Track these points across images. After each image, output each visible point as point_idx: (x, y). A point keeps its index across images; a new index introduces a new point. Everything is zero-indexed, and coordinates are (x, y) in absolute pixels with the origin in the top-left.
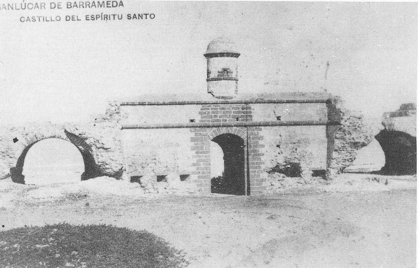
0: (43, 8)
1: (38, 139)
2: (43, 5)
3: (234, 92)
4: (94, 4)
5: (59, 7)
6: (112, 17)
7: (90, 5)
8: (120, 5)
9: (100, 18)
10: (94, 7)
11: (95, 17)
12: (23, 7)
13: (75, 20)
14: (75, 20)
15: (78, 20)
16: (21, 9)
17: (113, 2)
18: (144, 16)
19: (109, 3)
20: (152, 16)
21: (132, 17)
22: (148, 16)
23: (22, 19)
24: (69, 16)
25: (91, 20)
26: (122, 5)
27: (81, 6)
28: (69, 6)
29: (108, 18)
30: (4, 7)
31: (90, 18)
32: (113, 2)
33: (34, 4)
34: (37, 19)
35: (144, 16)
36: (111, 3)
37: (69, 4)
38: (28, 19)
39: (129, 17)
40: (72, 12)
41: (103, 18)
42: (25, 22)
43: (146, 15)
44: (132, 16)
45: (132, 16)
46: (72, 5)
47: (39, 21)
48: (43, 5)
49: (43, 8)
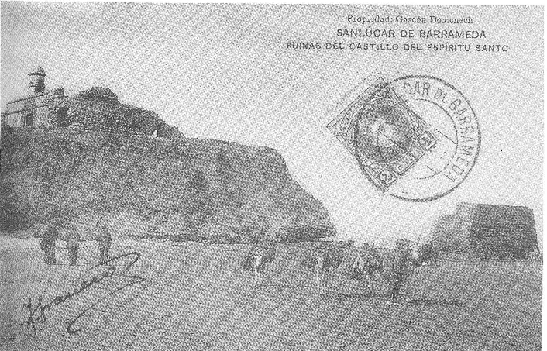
0: (392, 36)
3: (467, 111)
4: (346, 32)
5: (411, 35)
6: (458, 47)
7: (447, 35)
8: (481, 36)
10: (430, 36)
11: (439, 47)
12: (369, 34)
17: (473, 32)
18: (496, 48)
24: (330, 44)
25: (433, 50)
26: (484, 36)
27: (437, 36)
28: (423, 35)
29: (454, 48)
30: (430, 34)
31: (433, 48)
32: (473, 32)
33: (382, 31)
35: (496, 48)
36: (471, 33)
37: (422, 32)
38: (485, 48)
41: (448, 48)
42: (356, 49)
43: (498, 46)
44: (482, 48)
45: (482, 48)
47: (461, 50)
49: (392, 36)
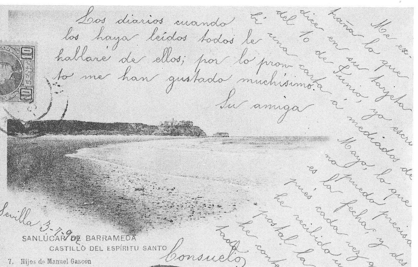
1: (399, 261)
2: (99, 237)
7: (107, 238)
9: (120, 249)
11: (115, 248)
13: (98, 250)
14: (98, 250)
15: (73, 250)
16: (43, 241)
19: (122, 237)
20: (164, 248)
21: (147, 249)
22: (161, 248)
23: (52, 249)
30: (93, 238)
31: (111, 249)
34: (65, 248)
38: (57, 249)
39: (145, 248)
40: (94, 243)
42: (54, 251)
46: (91, 238)
48: (99, 237)
